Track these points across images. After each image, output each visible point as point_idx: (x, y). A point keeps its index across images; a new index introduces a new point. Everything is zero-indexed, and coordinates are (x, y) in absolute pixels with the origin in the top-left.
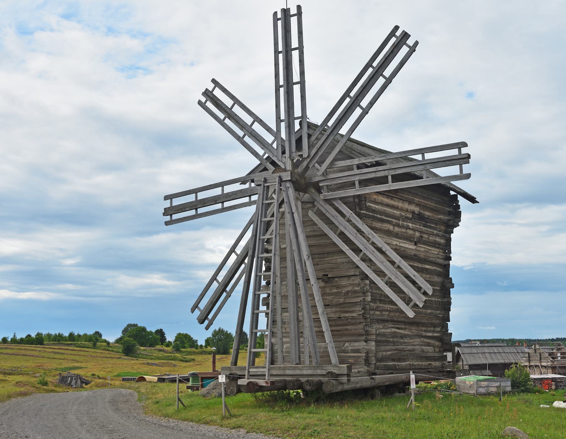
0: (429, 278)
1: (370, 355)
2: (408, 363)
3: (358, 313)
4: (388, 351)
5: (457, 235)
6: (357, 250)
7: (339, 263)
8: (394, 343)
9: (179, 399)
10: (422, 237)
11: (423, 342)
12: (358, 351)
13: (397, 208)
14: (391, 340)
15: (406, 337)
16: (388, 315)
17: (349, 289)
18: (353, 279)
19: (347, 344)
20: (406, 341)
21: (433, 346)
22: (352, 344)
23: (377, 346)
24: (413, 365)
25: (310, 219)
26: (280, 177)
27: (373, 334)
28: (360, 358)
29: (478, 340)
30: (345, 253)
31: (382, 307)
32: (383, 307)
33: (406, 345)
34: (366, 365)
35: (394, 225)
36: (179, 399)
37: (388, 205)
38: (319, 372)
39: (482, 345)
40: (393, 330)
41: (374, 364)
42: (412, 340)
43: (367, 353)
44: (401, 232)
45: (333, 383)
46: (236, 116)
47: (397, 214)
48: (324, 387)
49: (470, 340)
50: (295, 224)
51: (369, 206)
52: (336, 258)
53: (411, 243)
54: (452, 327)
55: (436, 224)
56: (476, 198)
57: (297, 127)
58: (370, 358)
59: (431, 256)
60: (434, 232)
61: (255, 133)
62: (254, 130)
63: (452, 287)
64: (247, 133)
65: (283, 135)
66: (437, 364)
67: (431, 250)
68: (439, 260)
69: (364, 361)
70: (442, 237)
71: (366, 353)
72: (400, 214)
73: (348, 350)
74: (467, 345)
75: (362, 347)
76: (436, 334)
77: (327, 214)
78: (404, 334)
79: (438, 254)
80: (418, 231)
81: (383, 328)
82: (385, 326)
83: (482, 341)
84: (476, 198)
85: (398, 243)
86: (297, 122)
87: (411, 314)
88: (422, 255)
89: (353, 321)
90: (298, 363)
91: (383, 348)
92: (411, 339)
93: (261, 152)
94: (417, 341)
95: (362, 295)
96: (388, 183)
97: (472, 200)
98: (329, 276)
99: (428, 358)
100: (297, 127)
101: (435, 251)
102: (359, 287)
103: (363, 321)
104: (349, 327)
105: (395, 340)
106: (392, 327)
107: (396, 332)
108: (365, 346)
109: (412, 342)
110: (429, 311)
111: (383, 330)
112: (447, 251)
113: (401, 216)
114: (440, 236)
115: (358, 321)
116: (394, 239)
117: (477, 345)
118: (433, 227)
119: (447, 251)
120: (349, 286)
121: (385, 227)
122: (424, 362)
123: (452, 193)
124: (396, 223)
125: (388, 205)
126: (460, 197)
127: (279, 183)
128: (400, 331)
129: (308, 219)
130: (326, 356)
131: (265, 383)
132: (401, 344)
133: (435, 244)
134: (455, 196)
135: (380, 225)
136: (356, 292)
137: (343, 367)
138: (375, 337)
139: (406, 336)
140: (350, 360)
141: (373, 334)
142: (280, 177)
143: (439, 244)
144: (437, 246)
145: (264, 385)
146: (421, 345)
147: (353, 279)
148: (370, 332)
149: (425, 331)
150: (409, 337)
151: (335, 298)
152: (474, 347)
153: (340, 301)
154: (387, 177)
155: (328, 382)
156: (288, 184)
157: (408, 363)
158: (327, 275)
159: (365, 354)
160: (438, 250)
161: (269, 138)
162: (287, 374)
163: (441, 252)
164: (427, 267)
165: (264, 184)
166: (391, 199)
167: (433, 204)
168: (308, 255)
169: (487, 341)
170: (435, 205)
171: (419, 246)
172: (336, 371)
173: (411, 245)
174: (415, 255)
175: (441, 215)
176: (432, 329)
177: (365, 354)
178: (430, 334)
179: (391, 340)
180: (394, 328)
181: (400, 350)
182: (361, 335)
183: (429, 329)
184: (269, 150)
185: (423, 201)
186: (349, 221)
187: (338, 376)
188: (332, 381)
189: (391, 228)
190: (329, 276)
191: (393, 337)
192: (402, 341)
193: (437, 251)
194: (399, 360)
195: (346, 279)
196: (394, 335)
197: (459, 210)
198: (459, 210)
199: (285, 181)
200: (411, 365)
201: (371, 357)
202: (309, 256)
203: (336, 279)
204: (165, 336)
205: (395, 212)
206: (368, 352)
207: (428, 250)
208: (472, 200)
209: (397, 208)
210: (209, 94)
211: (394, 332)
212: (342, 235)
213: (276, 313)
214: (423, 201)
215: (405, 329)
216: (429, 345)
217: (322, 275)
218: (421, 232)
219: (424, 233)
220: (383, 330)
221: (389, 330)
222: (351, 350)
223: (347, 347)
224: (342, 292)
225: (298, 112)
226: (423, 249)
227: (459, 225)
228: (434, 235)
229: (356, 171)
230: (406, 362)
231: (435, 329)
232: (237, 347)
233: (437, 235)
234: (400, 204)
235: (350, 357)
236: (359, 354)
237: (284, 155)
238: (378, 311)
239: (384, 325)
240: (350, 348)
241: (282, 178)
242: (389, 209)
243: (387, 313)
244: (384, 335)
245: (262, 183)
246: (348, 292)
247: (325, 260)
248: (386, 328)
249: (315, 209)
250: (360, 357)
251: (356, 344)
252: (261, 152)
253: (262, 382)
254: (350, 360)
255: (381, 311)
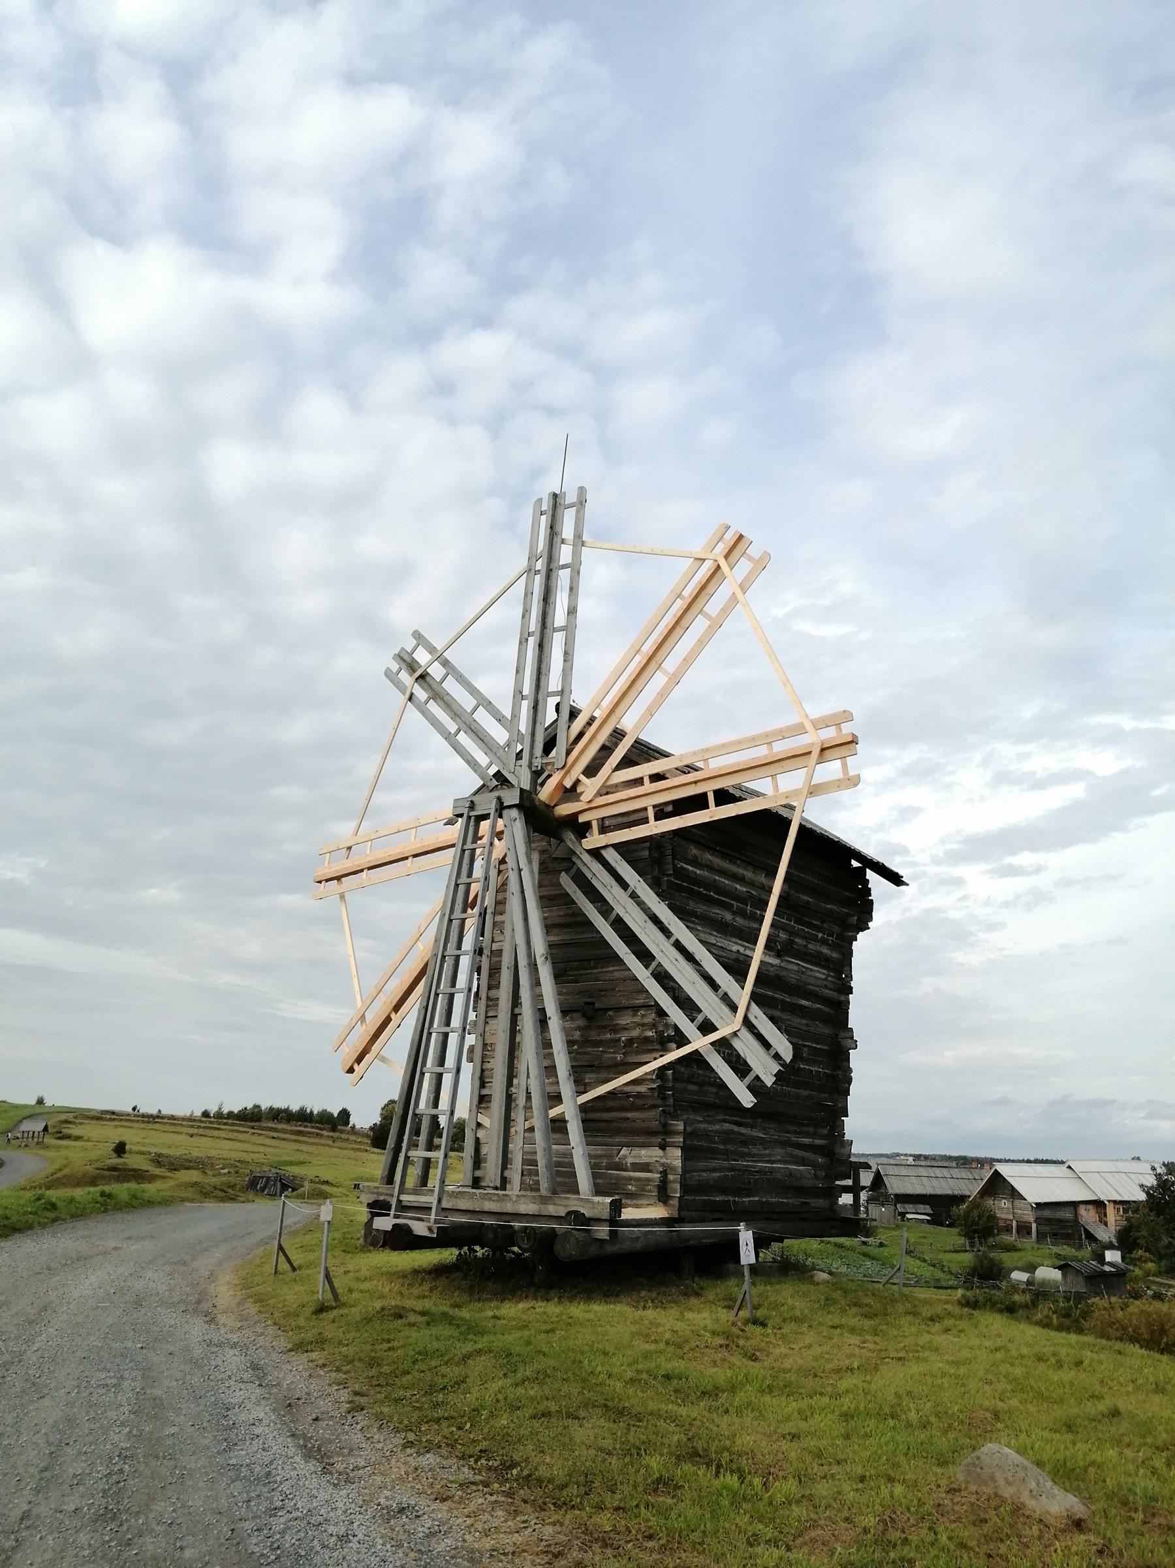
0: (807, 1025)
1: (671, 1177)
2: (756, 1199)
3: (649, 1087)
4: (714, 1170)
5: (862, 944)
6: (645, 956)
7: (617, 979)
8: (727, 1155)
9: (281, 1248)
10: (792, 942)
11: (792, 1156)
12: (645, 1167)
13: (742, 880)
14: (722, 1147)
15: (755, 1144)
16: (717, 1094)
17: (635, 1033)
18: (643, 1012)
19: (624, 1151)
20: (755, 1151)
21: (814, 1165)
22: (636, 1151)
23: (686, 1158)
24: (768, 1203)
25: (564, 892)
26: (499, 799)
27: (679, 1133)
28: (651, 1183)
29: (911, 1155)
30: (623, 960)
31: (702, 1075)
32: (706, 1076)
33: (754, 1161)
34: (661, 1199)
35: (734, 913)
36: (281, 1248)
37: (722, 872)
38: (551, 1210)
39: (917, 1163)
40: (727, 1126)
41: (677, 1199)
42: (767, 1152)
43: (664, 1173)
44: (748, 927)
45: (577, 1239)
46: (448, 697)
47: (741, 891)
48: (558, 1248)
49: (898, 1155)
50: (522, 892)
51: (682, 868)
52: (611, 968)
53: (769, 953)
54: (852, 1126)
55: (823, 922)
56: (902, 877)
57: (551, 716)
58: (671, 1185)
59: (812, 982)
60: (817, 936)
61: (478, 728)
62: (475, 721)
63: (854, 1046)
64: (463, 726)
65: (523, 726)
66: (821, 1203)
67: (812, 970)
68: (827, 991)
69: (656, 1190)
70: (833, 947)
71: (661, 1172)
72: (749, 892)
73: (626, 1163)
74: (892, 1162)
75: (655, 1159)
76: (818, 1142)
77: (594, 882)
78: (751, 1136)
79: (825, 979)
80: (784, 930)
81: (705, 1121)
82: (708, 1116)
83: (917, 1157)
84: (902, 877)
85: (742, 950)
86: (552, 702)
87: (747, 1100)
88: (792, 978)
89: (639, 1102)
90: (499, 1186)
91: (702, 1164)
92: (765, 1149)
93: (482, 759)
94: (779, 1152)
95: (660, 1047)
96: (708, 808)
97: (895, 879)
98: (597, 1006)
99: (800, 1191)
100: (551, 716)
101: (819, 973)
102: (654, 1031)
103: (659, 1102)
104: (629, 1115)
105: (729, 1147)
106: (725, 1121)
107: (732, 1132)
108: (661, 1157)
109: (766, 1155)
110: (806, 1093)
111: (703, 1126)
112: (844, 976)
113: (751, 896)
114: (830, 945)
115: (651, 1102)
116: (734, 940)
117: (908, 1163)
118: (816, 925)
119: (844, 976)
120: (634, 1028)
121: (714, 913)
122: (791, 1198)
123: (855, 864)
124: (738, 908)
125: (722, 872)
126: (870, 875)
127: (496, 811)
128: (743, 1130)
129: (558, 892)
130: (564, 1180)
131: (427, 1229)
132: (743, 1156)
133: (818, 960)
134: (861, 872)
135: (704, 908)
136: (647, 1040)
137: (603, 1204)
138: (682, 1140)
139: (753, 1141)
140: (630, 1187)
141: (679, 1133)
142: (499, 799)
143: (828, 959)
144: (823, 963)
145: (426, 1233)
146: (786, 1162)
147: (643, 1012)
148: (673, 1128)
149: (796, 1133)
150: (760, 1144)
151: (606, 1052)
152: (905, 1165)
153: (616, 1058)
154: (705, 795)
155: (567, 1233)
156: (514, 813)
157: (756, 1199)
158: (593, 1004)
159: (659, 1176)
160: (825, 972)
161: (500, 735)
162: (486, 1210)
163: (832, 976)
164: (804, 1002)
165: (468, 813)
166: (730, 861)
167: (816, 881)
168: (543, 955)
169: (926, 1158)
170: (819, 882)
171: (786, 961)
172: (587, 1212)
173: (770, 956)
174: (778, 977)
175: (834, 904)
176: (811, 1129)
177: (659, 1176)
178: (806, 1140)
179: (722, 1147)
180: (729, 1122)
181: (740, 1170)
182: (654, 1133)
183: (805, 1129)
184: (498, 758)
185: (795, 873)
186: (634, 896)
187: (592, 1222)
188: (575, 1232)
189: (728, 917)
190: (597, 1006)
191: (725, 1142)
192: (746, 1150)
193: (824, 974)
194: (739, 1192)
195: (630, 1012)
196: (728, 1137)
197: (870, 898)
198: (870, 898)
199: (510, 807)
200: (763, 1203)
201: (671, 1182)
202: (546, 958)
203: (610, 1013)
204: (308, 1111)
205: (738, 887)
206: (666, 1170)
207: (804, 970)
208: (895, 879)
209: (742, 880)
210: (406, 657)
211: (729, 1130)
212: (620, 926)
213: (492, 1078)
214: (795, 873)
215: (752, 1127)
216: (802, 1162)
217: (583, 1004)
218: (792, 933)
219: (796, 934)
220: (703, 1126)
221: (717, 1127)
222: (632, 1164)
223: (625, 1157)
224: (619, 1040)
225: (554, 682)
226: (795, 968)
227: (869, 928)
228: (818, 941)
229: (648, 786)
230: (753, 1196)
231: (818, 1130)
232: (396, 1145)
233: (824, 942)
234: (749, 874)
235: (631, 1179)
236: (649, 1175)
237: (519, 762)
238: (694, 1084)
239: (705, 1114)
240: (630, 1160)
241: (503, 800)
242: (725, 879)
243: (715, 1090)
244: (706, 1135)
245: (465, 811)
246: (630, 1041)
247: (591, 973)
248: (710, 1123)
249: (573, 871)
250: (648, 1180)
251: (643, 1152)
252: (482, 759)
253: (420, 1229)
254: (630, 1187)
255: (701, 1085)
